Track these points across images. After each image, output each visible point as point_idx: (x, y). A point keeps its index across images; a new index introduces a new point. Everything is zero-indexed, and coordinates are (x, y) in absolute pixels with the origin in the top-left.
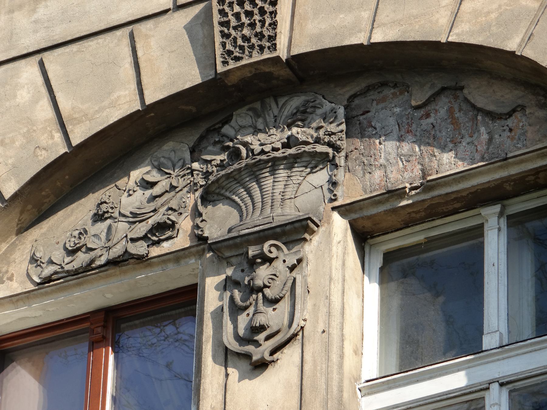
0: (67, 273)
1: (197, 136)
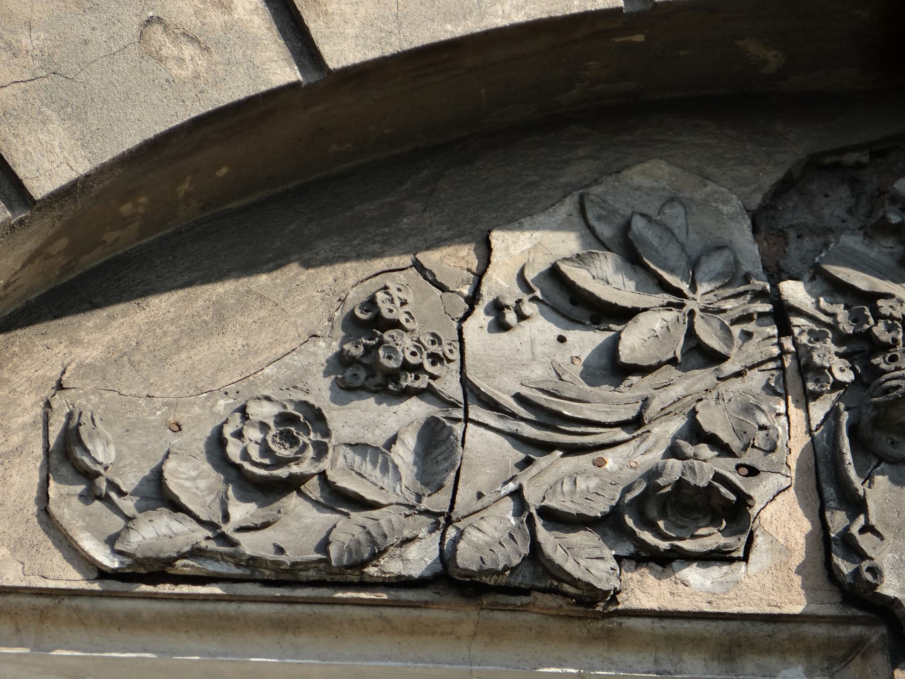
0: (247, 566)
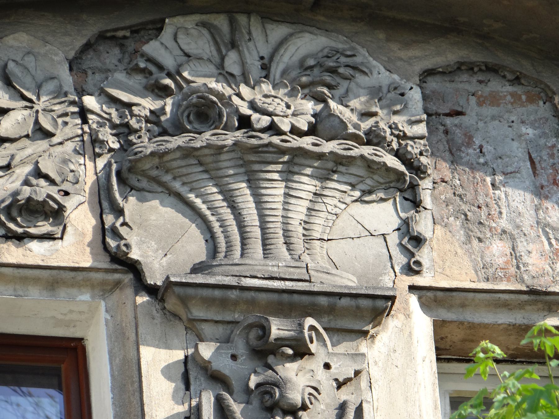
1: (80, 42)
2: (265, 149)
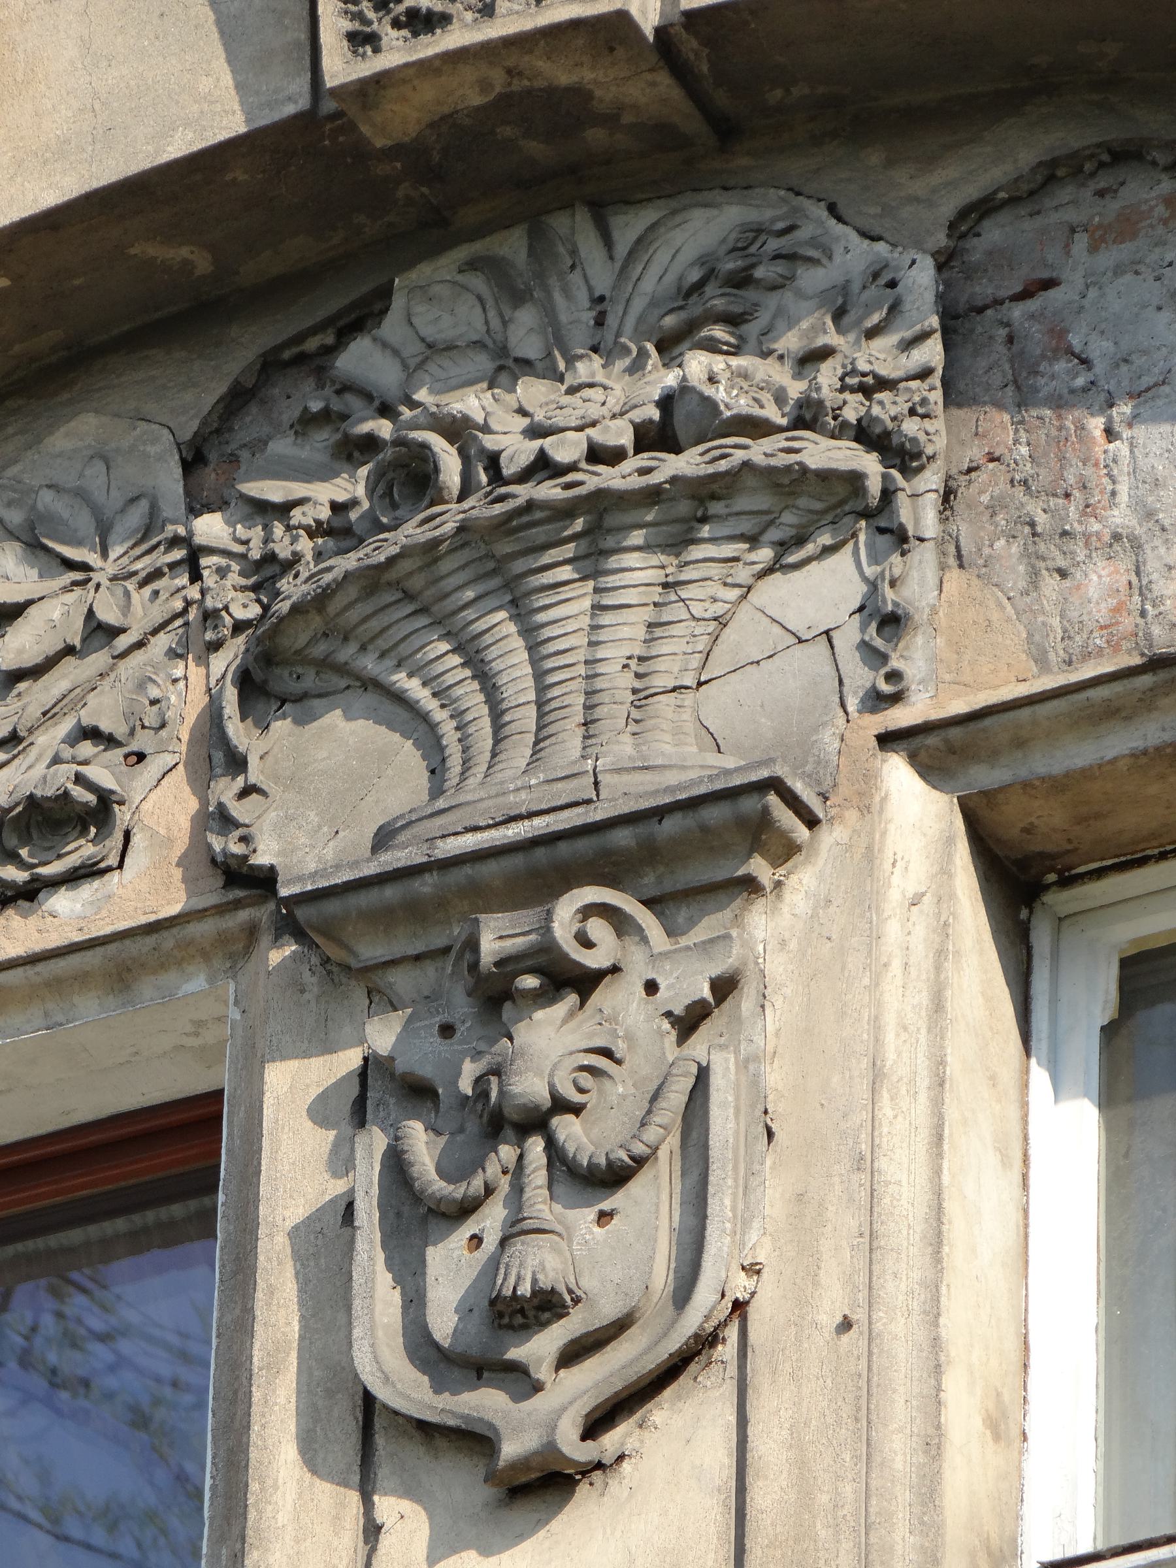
2: (525, 519)
